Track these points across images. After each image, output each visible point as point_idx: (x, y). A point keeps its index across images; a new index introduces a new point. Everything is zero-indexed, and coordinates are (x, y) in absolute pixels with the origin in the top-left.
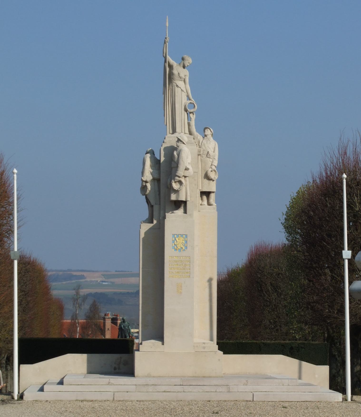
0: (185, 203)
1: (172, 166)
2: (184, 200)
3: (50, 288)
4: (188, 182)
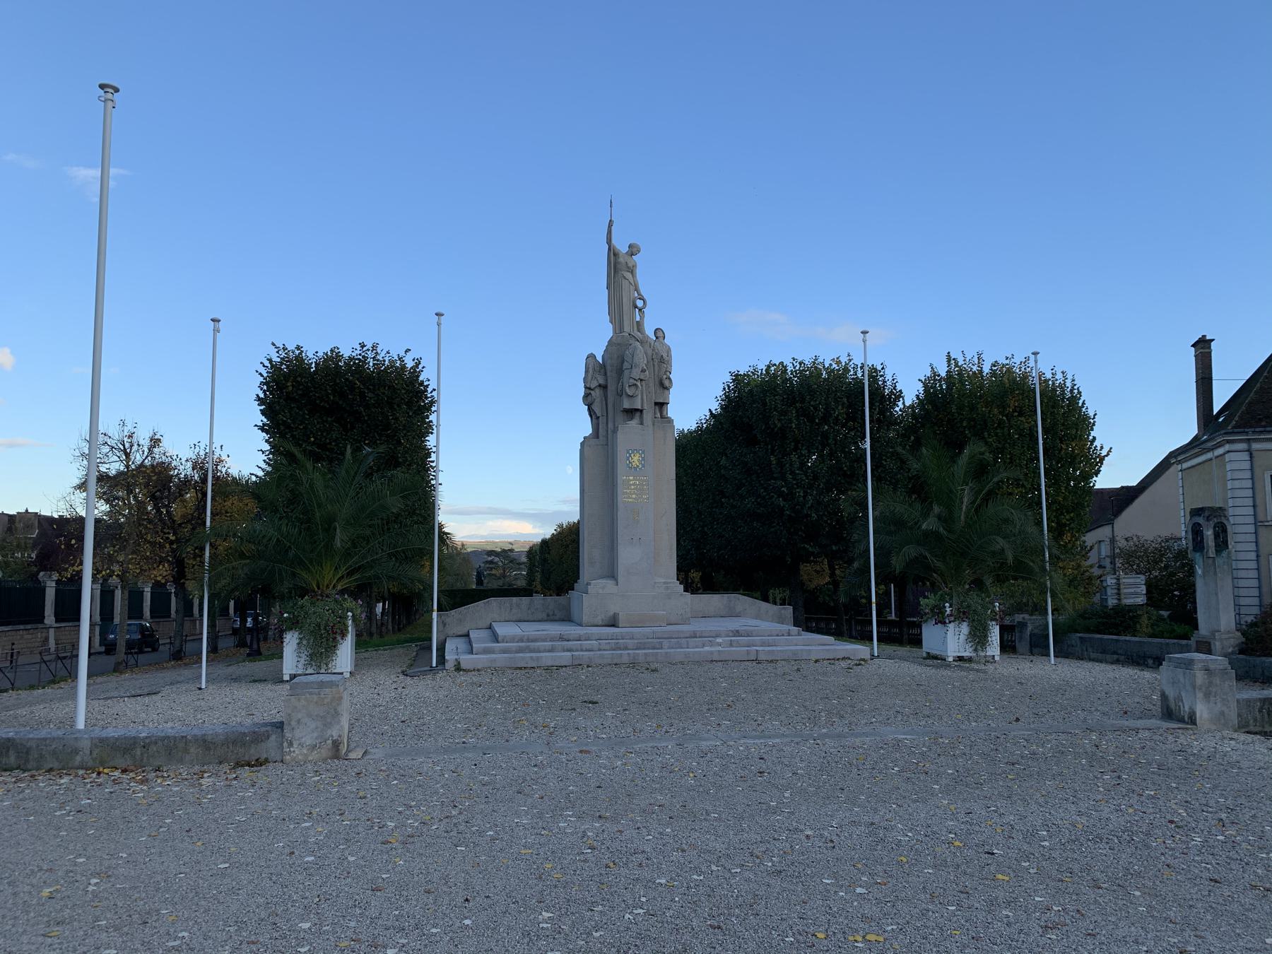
0: (641, 411)
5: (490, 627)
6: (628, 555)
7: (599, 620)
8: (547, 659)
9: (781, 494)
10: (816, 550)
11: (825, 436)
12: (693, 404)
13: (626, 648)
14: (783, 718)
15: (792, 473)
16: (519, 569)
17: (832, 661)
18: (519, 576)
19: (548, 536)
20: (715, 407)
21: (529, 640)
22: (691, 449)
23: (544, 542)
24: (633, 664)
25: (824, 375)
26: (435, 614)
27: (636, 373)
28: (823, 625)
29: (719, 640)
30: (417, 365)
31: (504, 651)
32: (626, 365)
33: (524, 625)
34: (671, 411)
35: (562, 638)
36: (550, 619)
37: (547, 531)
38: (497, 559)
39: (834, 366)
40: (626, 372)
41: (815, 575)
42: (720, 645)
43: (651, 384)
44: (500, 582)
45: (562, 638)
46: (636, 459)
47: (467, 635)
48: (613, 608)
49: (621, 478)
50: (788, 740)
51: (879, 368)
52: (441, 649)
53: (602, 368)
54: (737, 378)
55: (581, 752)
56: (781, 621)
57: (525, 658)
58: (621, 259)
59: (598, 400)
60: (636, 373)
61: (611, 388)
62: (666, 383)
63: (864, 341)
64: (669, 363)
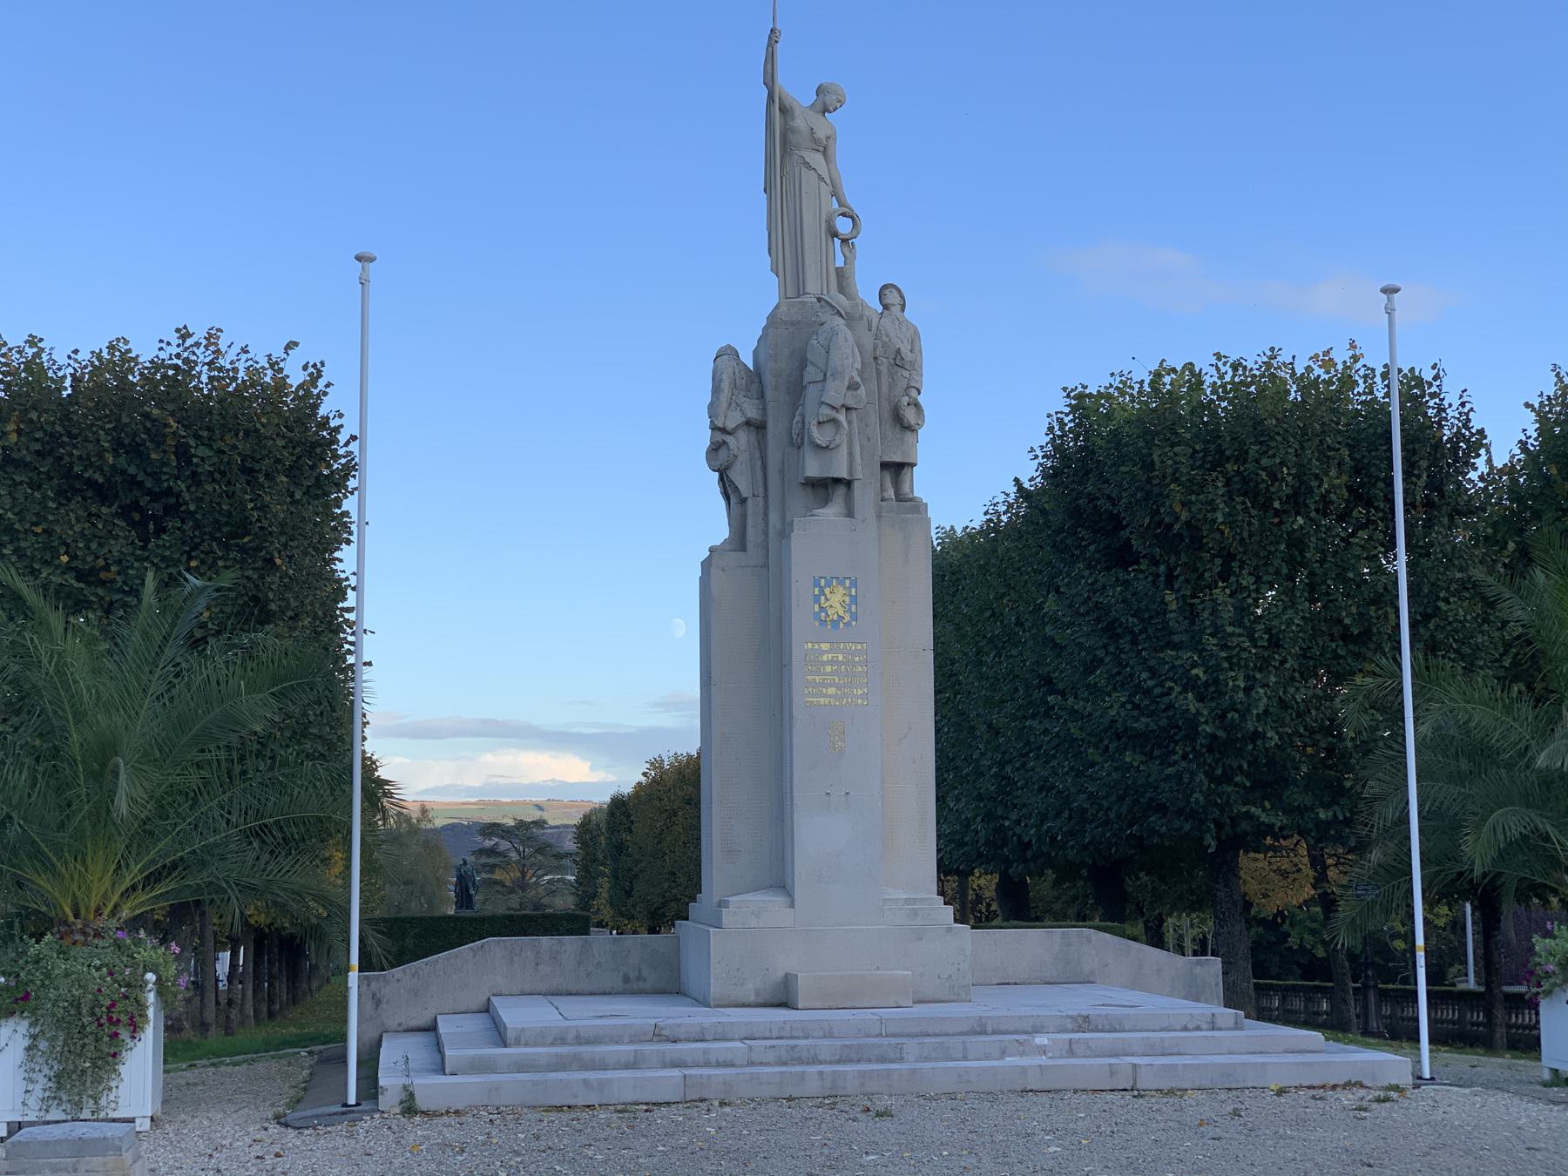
0: (848, 484)
1: (807, 378)
2: (844, 474)
3: (349, 469)
4: (855, 425)
5: (487, 1009)
6: (817, 835)
7: (748, 992)
8: (624, 1085)
9: (1190, 684)
10: (1278, 819)
11: (1297, 542)
12: (975, 466)
13: (814, 1060)
17: (1320, 1090)
18: (558, 887)
19: (627, 789)
20: (1029, 472)
21: (580, 1040)
23: (619, 805)
24: (832, 1100)
25: (1294, 394)
26: (354, 977)
27: (835, 392)
28: (1298, 1004)
29: (1042, 1040)
31: (521, 1067)
32: (811, 373)
33: (566, 1003)
34: (921, 484)
35: (658, 1035)
36: (631, 987)
37: (626, 777)
38: (504, 845)
39: (1318, 371)
40: (812, 392)
41: (1276, 880)
42: (1043, 1050)
43: (873, 419)
44: (514, 901)
45: (658, 1035)
46: (836, 600)
47: (432, 1028)
48: (784, 962)
51: (1428, 375)
52: (369, 1062)
53: (754, 381)
54: (1082, 403)
56: (1194, 993)
57: (572, 1084)
58: (799, 123)
62: (910, 415)
63: (1390, 311)
64: (915, 367)
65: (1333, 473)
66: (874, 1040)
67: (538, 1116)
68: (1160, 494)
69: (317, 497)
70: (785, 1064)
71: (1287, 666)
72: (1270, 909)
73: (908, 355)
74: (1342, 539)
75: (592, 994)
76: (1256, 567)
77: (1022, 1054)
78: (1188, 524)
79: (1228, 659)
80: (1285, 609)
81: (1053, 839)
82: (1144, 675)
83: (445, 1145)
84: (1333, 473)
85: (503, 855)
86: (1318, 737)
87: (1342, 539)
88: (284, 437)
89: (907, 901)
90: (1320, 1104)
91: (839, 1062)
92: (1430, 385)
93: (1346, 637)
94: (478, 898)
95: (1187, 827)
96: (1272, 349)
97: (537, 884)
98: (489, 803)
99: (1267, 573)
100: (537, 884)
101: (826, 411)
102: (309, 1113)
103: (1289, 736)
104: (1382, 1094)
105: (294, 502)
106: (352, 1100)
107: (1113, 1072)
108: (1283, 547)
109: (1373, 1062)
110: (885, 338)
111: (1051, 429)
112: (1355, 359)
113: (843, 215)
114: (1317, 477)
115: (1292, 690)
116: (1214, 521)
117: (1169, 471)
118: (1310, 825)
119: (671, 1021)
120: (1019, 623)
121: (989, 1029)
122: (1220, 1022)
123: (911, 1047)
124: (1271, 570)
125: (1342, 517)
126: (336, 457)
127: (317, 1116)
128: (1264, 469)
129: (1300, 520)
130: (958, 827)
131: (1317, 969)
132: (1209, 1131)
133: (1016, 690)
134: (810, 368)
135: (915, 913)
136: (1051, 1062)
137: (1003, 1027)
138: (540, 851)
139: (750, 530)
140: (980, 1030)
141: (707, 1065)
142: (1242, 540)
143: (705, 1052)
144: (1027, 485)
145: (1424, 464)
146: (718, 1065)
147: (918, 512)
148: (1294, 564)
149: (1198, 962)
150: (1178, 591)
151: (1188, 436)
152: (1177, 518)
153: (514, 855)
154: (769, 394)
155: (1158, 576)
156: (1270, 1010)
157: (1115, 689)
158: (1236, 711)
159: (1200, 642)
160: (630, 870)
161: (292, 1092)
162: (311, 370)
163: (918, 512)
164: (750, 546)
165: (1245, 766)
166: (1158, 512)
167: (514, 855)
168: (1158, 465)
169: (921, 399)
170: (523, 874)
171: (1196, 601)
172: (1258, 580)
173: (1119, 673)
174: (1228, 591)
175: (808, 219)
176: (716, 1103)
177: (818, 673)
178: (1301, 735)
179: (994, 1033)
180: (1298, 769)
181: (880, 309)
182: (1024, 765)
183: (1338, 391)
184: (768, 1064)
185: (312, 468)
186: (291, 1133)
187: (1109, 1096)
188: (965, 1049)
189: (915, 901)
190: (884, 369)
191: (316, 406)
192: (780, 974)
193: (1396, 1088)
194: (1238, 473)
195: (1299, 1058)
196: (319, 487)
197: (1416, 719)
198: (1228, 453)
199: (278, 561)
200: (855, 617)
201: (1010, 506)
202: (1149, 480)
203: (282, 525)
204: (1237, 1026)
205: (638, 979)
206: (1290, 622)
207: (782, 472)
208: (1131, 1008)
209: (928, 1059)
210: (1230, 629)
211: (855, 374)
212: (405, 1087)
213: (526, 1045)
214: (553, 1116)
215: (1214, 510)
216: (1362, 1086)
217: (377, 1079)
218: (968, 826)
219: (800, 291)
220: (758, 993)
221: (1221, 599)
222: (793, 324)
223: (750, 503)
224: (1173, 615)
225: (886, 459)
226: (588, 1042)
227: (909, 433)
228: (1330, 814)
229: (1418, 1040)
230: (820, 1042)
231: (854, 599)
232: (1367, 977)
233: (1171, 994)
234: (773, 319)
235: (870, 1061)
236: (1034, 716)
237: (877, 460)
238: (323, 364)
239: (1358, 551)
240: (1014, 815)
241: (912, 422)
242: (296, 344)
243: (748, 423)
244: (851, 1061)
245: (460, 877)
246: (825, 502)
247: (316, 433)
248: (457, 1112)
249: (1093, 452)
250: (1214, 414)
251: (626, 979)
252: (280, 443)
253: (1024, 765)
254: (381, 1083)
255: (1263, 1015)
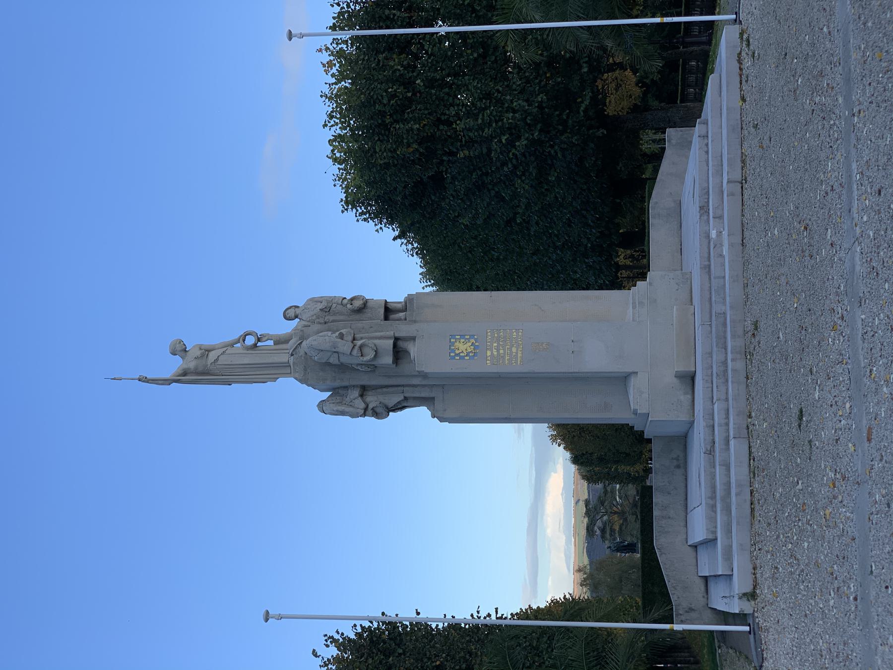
0: (397, 339)
1: (337, 362)
2: (391, 342)
5: (695, 547)
6: (596, 358)
7: (685, 399)
8: (739, 473)
9: (511, 143)
10: (588, 94)
11: (431, 83)
12: (387, 266)
13: (725, 363)
14: (823, 155)
15: (481, 128)
16: (613, 491)
17: (743, 78)
18: (622, 494)
19: (568, 455)
20: (390, 232)
21: (713, 497)
22: (452, 268)
23: (576, 460)
24: (747, 354)
25: (347, 84)
26: (677, 627)
27: (345, 347)
28: (692, 78)
29: (713, 234)
30: (335, 641)
31: (728, 531)
32: (334, 360)
33: (692, 504)
34: (396, 297)
35: (710, 452)
36: (682, 464)
37: (561, 456)
38: (599, 523)
39: (334, 70)
40: (344, 359)
41: (621, 93)
42: (719, 233)
43: (360, 325)
44: (631, 518)
45: (710, 452)
46: (463, 347)
47: (706, 579)
48: (669, 378)
49: (488, 367)
50: (853, 152)
51: (337, 9)
52: (726, 617)
53: (338, 392)
54: (351, 202)
55: (869, 440)
56: (687, 144)
57: (739, 503)
58: (192, 365)
59: (381, 398)
60: (345, 347)
61: (365, 380)
62: (358, 304)
63: (302, 36)
64: (331, 300)
65: (392, 63)
66: (714, 329)
67: (757, 522)
68: (403, 159)
69: (401, 640)
70: (727, 381)
71: (501, 89)
72: (637, 91)
73: (324, 304)
74: (429, 58)
75: (686, 487)
76: (445, 106)
77: (722, 245)
78: (420, 144)
79: (496, 122)
80: (468, 90)
81: (598, 219)
82: (506, 169)
83: (773, 577)
84: (392, 63)
85: (605, 524)
86: (541, 72)
87: (429, 58)
88: (367, 659)
89: (634, 307)
90: (750, 78)
91: (726, 349)
92: (343, 8)
93: (484, 56)
94: (629, 540)
95: (592, 145)
96: (321, 96)
97: (622, 505)
98: (575, 531)
99: (448, 100)
100: (622, 505)
101: (355, 352)
102: (754, 653)
103: (540, 87)
104: (745, 43)
105: (404, 653)
106: (747, 628)
107: (731, 194)
108: (433, 91)
109: (727, 47)
110: (314, 317)
111: (365, 220)
112: (327, 49)
113: (244, 341)
114: (394, 72)
115: (514, 86)
116: (418, 129)
117: (390, 154)
118: (591, 76)
119: (702, 445)
120: (475, 238)
121: (707, 263)
122: (703, 133)
123: (717, 308)
124: (446, 97)
125: (416, 57)
126: (378, 628)
127: (756, 649)
128: (389, 101)
129: (418, 81)
130: (591, 272)
131: (671, 66)
132: (766, 142)
133: (513, 239)
134: (331, 360)
135: (641, 303)
136: (726, 228)
137: (706, 255)
138: (602, 503)
139: (423, 395)
140: (707, 269)
141: (727, 424)
142: (429, 114)
143: (720, 425)
144: (397, 233)
145: (387, 12)
146: (727, 418)
147: (413, 299)
148: (443, 84)
149: (669, 141)
150: (457, 149)
151: (370, 144)
152: (417, 150)
153: (605, 518)
154: (346, 383)
155: (449, 160)
156: (695, 94)
157: (514, 185)
158: (526, 117)
159: (487, 138)
160: (614, 454)
161: (742, 660)
162: (329, 643)
163: (413, 299)
164: (432, 395)
165: (557, 113)
166: (413, 161)
167: (605, 518)
168: (386, 161)
169: (348, 298)
170: (615, 513)
171: (464, 139)
172: (452, 105)
173: (505, 183)
174: (458, 122)
175: (246, 361)
176: (749, 420)
177: (503, 357)
178: (541, 81)
179: (709, 261)
180: (559, 83)
181: (297, 320)
182: (557, 236)
183: (345, 59)
184: (727, 389)
185: (385, 643)
186: (765, 664)
187: (746, 197)
188: (719, 277)
189: (634, 303)
190: (331, 318)
191: (350, 640)
192: (676, 381)
193: (741, 34)
194: (391, 115)
195: (724, 88)
196: (396, 638)
197: (532, 22)
198: (380, 121)
199: (438, 663)
200: (472, 336)
201: (408, 241)
202: (395, 166)
203: (417, 660)
204: (706, 123)
205: (678, 460)
206: (476, 88)
207: (390, 377)
208: (696, 179)
209: (724, 299)
210: (480, 121)
211: (334, 335)
212: (740, 598)
213: (716, 527)
214: (757, 514)
215: (412, 129)
216: (740, 54)
217: (734, 614)
218: (590, 266)
219: (286, 365)
220: (685, 393)
221: (462, 126)
222: (305, 370)
223: (407, 395)
224: (472, 153)
225: (382, 317)
226: (714, 492)
227: (369, 304)
228: (585, 65)
229: (713, 21)
230: (714, 359)
231: (462, 336)
232: (677, 43)
233: (687, 157)
234: (303, 381)
235: (725, 332)
236: (528, 229)
237: (383, 322)
238: (326, 635)
239: (436, 49)
240: (585, 241)
241: (362, 302)
242: (314, 651)
243: (362, 396)
244: (725, 342)
245: (617, 550)
246: (407, 352)
247: (365, 640)
248: (754, 569)
249: (378, 196)
250: (358, 129)
251: (678, 467)
252: (370, 661)
253: (557, 236)
254: (737, 612)
255: (700, 98)
